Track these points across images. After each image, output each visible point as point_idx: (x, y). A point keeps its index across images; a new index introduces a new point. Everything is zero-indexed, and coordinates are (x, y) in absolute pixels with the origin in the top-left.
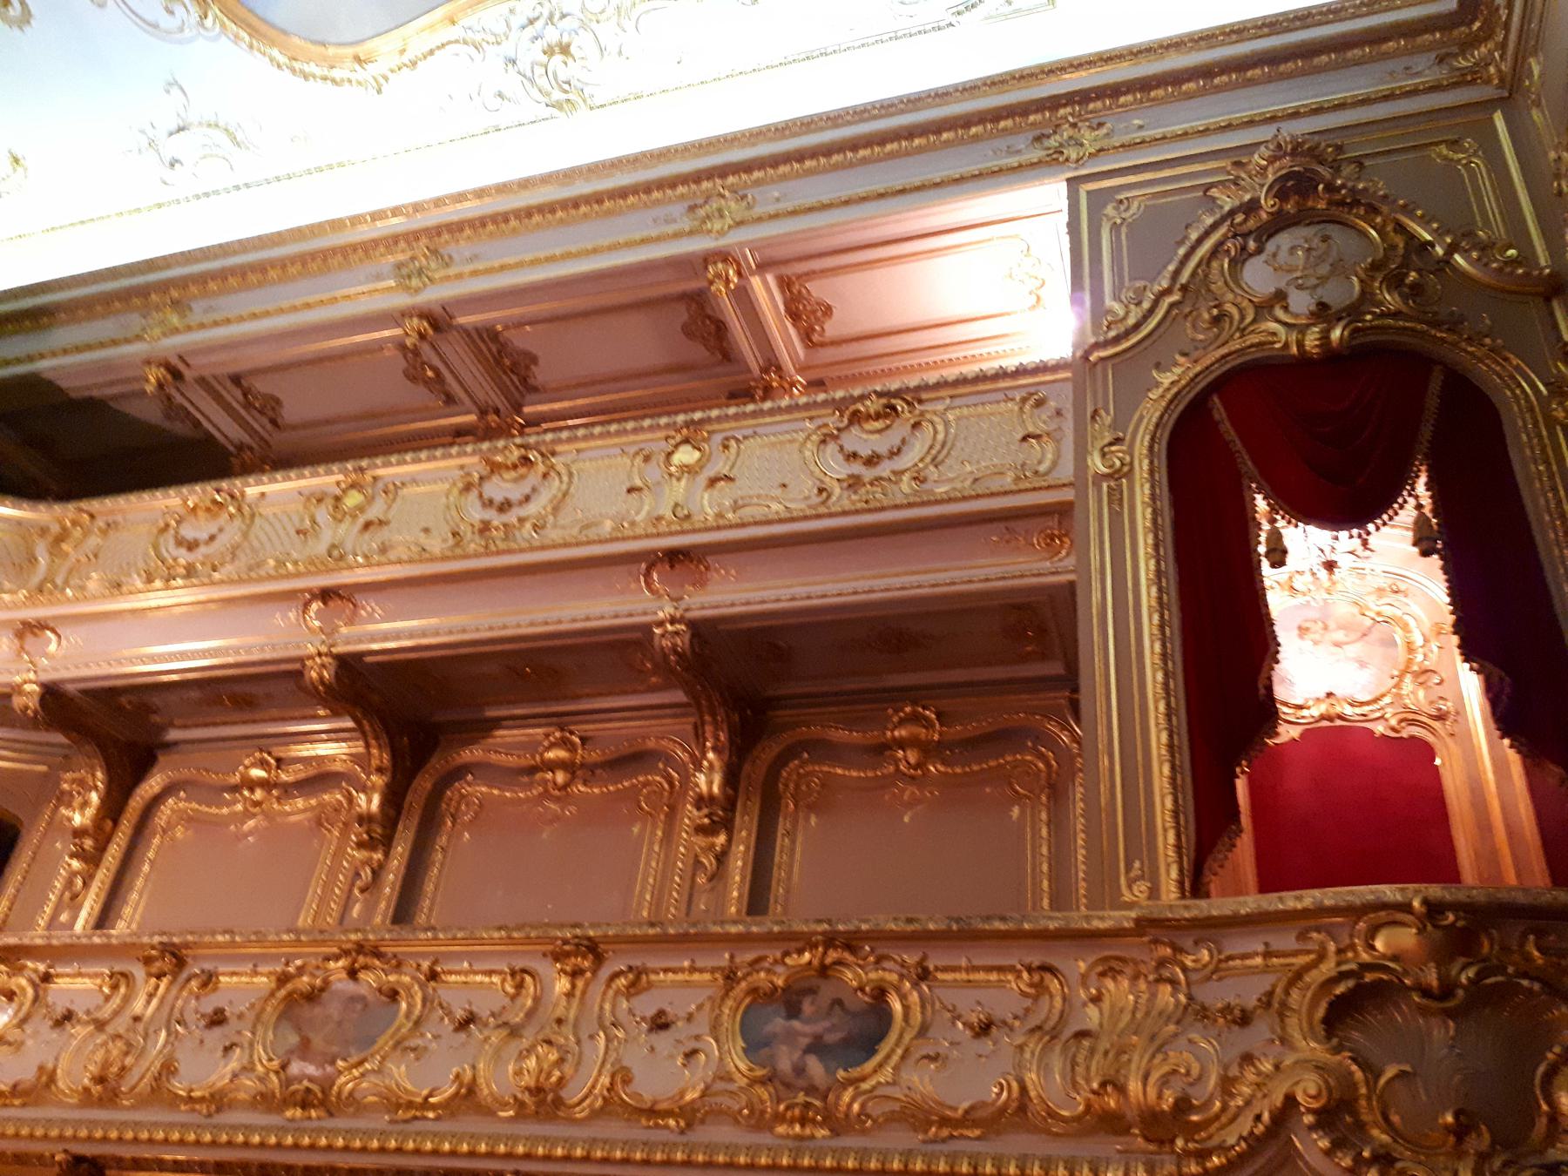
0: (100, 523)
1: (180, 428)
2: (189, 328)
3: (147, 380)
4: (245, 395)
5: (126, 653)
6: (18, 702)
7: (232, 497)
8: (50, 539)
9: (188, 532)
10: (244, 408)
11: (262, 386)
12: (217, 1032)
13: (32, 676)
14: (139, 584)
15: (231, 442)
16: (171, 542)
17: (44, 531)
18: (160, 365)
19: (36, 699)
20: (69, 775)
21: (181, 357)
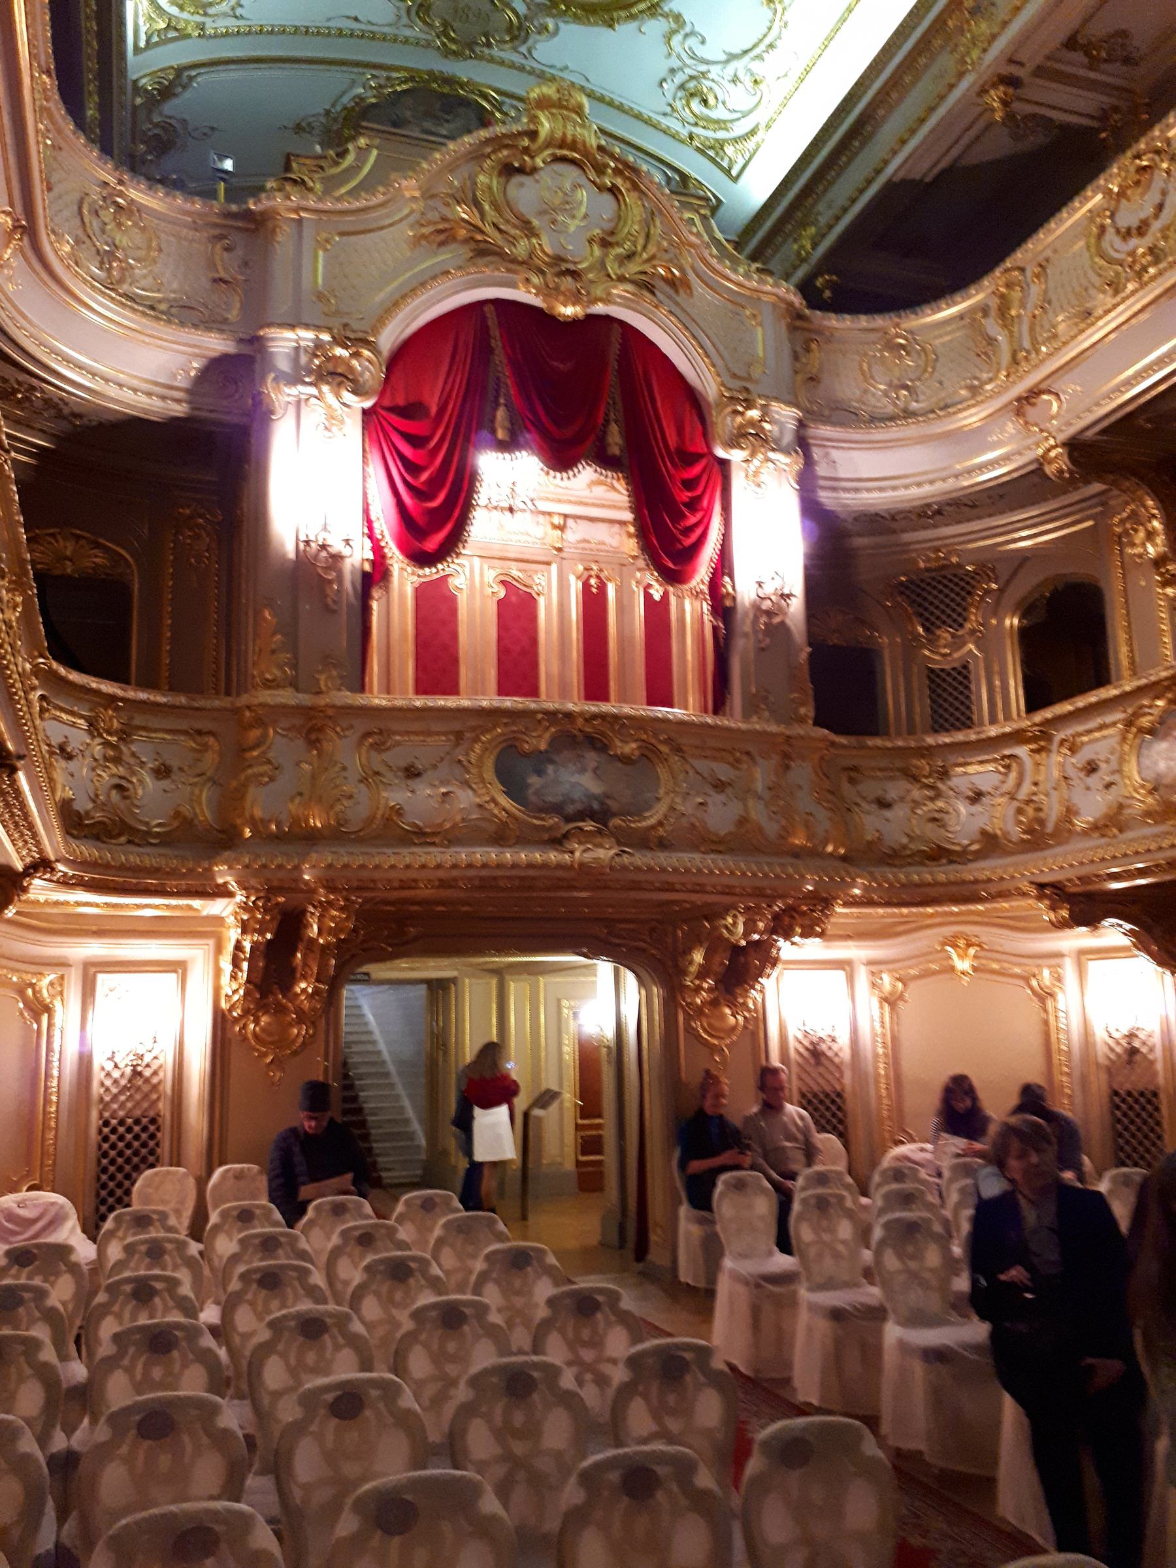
0: (1032, 269)
1: (1037, 139)
2: (1005, 24)
3: (993, 110)
4: (1087, 54)
5: (1106, 388)
7: (1158, 152)
9: (1128, 217)
10: (1091, 68)
11: (1099, 29)
13: (1052, 442)
14: (1110, 301)
15: (1092, 117)
16: (1118, 242)
17: (985, 310)
18: (994, 86)
20: (1116, 520)
21: (1011, 61)
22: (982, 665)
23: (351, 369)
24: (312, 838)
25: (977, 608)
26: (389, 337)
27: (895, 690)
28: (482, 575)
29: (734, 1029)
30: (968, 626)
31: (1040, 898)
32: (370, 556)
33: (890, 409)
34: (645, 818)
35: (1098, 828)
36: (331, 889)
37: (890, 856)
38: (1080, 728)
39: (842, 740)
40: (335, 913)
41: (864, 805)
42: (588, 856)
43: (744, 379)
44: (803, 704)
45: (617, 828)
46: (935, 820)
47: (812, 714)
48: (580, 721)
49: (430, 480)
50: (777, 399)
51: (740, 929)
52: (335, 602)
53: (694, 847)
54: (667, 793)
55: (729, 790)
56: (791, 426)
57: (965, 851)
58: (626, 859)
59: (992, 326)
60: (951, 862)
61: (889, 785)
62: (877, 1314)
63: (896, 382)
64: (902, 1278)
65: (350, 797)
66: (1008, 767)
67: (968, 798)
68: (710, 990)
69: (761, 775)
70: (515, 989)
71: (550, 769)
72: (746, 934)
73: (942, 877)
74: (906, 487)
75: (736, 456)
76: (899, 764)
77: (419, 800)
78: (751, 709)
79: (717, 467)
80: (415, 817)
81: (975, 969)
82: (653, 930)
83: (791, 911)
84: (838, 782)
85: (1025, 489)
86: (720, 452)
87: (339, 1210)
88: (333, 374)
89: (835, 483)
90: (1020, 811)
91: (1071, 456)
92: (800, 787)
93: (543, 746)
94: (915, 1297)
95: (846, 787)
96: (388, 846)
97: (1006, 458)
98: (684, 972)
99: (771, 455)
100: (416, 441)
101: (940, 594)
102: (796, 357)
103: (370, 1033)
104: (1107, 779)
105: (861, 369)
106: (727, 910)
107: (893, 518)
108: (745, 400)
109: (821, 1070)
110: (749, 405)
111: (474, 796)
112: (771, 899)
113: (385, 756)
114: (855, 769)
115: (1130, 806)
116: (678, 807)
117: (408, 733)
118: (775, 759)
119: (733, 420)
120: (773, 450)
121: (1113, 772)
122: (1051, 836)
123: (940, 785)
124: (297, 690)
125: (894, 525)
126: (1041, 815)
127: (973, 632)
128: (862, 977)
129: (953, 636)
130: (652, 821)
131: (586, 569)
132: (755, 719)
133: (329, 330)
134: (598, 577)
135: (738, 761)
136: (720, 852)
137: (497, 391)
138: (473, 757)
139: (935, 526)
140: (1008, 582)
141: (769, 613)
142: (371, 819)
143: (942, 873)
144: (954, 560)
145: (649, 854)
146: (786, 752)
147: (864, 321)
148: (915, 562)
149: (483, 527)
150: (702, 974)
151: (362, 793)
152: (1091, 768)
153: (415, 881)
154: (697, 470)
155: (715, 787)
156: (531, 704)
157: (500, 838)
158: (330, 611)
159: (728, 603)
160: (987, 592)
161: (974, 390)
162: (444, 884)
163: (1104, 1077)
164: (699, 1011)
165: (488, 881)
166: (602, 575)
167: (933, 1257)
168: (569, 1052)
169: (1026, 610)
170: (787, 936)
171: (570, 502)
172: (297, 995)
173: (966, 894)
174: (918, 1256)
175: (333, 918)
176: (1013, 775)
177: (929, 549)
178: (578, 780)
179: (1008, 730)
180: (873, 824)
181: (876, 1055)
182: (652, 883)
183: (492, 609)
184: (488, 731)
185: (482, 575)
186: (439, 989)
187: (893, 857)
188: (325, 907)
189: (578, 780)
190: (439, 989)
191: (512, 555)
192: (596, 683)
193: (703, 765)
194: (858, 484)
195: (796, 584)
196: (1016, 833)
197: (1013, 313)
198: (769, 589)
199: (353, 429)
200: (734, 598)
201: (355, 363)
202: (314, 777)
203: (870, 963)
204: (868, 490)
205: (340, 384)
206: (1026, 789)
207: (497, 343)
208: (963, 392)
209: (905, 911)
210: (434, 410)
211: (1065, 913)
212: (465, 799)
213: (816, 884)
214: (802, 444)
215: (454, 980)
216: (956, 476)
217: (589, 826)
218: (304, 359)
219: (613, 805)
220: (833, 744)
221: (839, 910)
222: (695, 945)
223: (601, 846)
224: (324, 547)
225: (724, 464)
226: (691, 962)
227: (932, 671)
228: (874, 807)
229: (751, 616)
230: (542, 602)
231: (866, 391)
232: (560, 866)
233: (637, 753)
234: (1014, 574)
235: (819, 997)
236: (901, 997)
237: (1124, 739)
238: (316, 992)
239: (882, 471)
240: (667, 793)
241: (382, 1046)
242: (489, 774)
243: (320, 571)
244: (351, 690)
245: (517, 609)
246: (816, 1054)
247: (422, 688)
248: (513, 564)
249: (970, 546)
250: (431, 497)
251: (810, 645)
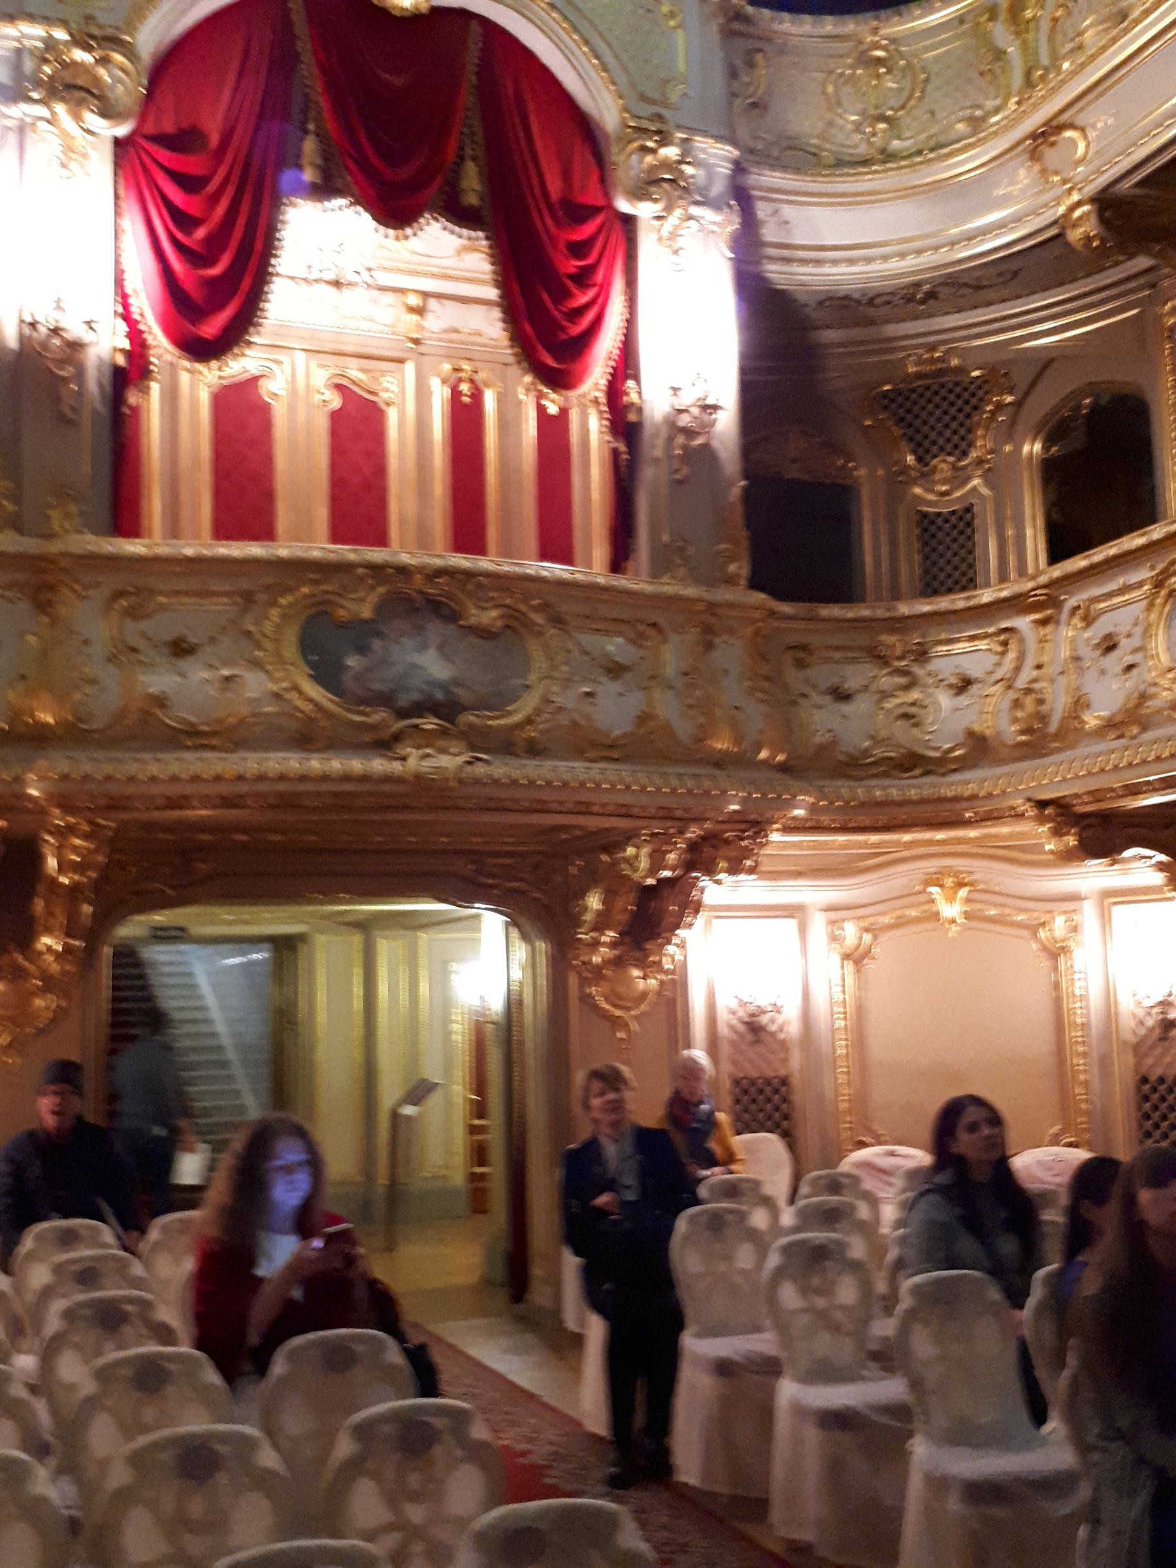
6: (1075, 236)
8: (1003, 16)
12: (1114, 655)
13: (1076, 197)
19: (1093, 219)
22: (990, 506)
23: (97, 80)
24: (41, 739)
25: (987, 429)
26: (153, 34)
27: (874, 543)
28: (308, 376)
29: (644, 995)
30: (974, 454)
31: (1041, 819)
32: (126, 344)
33: (863, 150)
34: (510, 713)
35: (1113, 726)
36: (67, 807)
37: (847, 765)
38: (1097, 591)
39: (786, 608)
40: (78, 842)
41: (816, 698)
42: (428, 764)
43: (653, 102)
44: (732, 559)
45: (471, 726)
46: (906, 716)
47: (745, 572)
48: (418, 579)
49: (209, 240)
50: (705, 133)
51: (644, 864)
52: (73, 408)
53: (578, 753)
54: (541, 679)
55: (628, 676)
56: (725, 169)
57: (943, 761)
58: (480, 769)
59: (1000, 32)
60: (928, 773)
61: (849, 670)
62: (771, 1368)
63: (872, 112)
64: (805, 1319)
65: (93, 681)
66: (1005, 644)
67: (951, 686)
68: (613, 945)
69: (672, 656)
70: (386, 948)
71: (377, 644)
72: (652, 871)
73: (913, 793)
74: (885, 258)
75: (644, 210)
76: (864, 640)
77: (190, 687)
78: (660, 566)
79: (618, 225)
80: (181, 714)
81: (967, 915)
82: (537, 866)
83: (711, 840)
84: (778, 666)
85: (1040, 264)
86: (623, 205)
87: (68, 1239)
88: (70, 87)
89: (789, 253)
90: (1017, 704)
91: (1102, 220)
92: (726, 672)
93: (366, 612)
94: (823, 1344)
95: (793, 676)
96: (144, 749)
97: (1017, 219)
98: (575, 922)
99: (694, 210)
100: (188, 183)
101: (938, 409)
102: (733, 74)
103: (203, 1008)
104: (1129, 659)
105: (824, 93)
106: (629, 837)
107: (871, 302)
108: (659, 132)
109: (761, 1049)
110: (665, 140)
111: (268, 680)
112: (684, 822)
113: (144, 625)
114: (804, 647)
115: (1153, 696)
116: (558, 699)
117: (177, 593)
118: (693, 633)
119: (641, 161)
120: (697, 203)
121: (1136, 651)
122: (1056, 736)
123: (917, 670)
124: (20, 531)
125: (871, 312)
126: (1044, 708)
127: (980, 462)
128: (818, 924)
129: (955, 468)
130: (517, 718)
131: (456, 370)
132: (665, 579)
133: (64, 23)
134: (472, 381)
135: (642, 636)
136: (616, 760)
137: (305, 112)
138: (268, 627)
139: (931, 316)
140: (1027, 394)
141: (689, 432)
142: (122, 713)
143: (915, 787)
144: (955, 362)
145: (515, 762)
146: (709, 625)
147: (829, 25)
148: (902, 362)
149: (283, 303)
150: (600, 925)
151: (109, 676)
152: (1109, 645)
153: (186, 797)
154: (589, 228)
155: (609, 671)
156: (376, 555)
157: (305, 738)
158: (66, 421)
159: (632, 417)
160: (1000, 407)
161: (977, 124)
162: (228, 802)
163: (1130, 1059)
164: (597, 974)
165: (288, 798)
166: (476, 377)
167: (847, 1292)
168: (460, 1032)
169: (1054, 433)
170: (710, 871)
171: (434, 276)
172: (40, 953)
173: (943, 813)
174: (826, 1291)
175: (75, 849)
176: (1012, 655)
177: (922, 346)
178: (428, 662)
179: (1004, 594)
180: (824, 721)
181: (834, 1031)
182: (517, 801)
183: (322, 424)
184: (290, 590)
185: (308, 376)
186: (285, 948)
187: (853, 766)
188: (63, 833)
189: (428, 662)
190: (285, 948)
191: (349, 349)
192: (468, 530)
193: (590, 641)
194: (819, 253)
195: (725, 392)
196: (1011, 732)
197: (1029, 14)
198: (687, 399)
199: (100, 168)
200: (640, 410)
201: (102, 72)
202: (44, 653)
203: (829, 908)
204: (835, 262)
205: (80, 103)
206: (1027, 674)
207: (304, 47)
208: (961, 127)
209: (874, 838)
210: (214, 140)
211: (1071, 841)
212: (255, 684)
213: (744, 801)
214: (741, 197)
215: (301, 938)
216: (953, 244)
217: (430, 723)
218: (29, 65)
219: (464, 695)
220: (772, 613)
221: (775, 837)
222: (606, 890)
223: (444, 751)
224: (56, 331)
225: (629, 221)
226: (586, 909)
227: (925, 515)
228: (827, 699)
229: (664, 434)
230: (392, 416)
231: (831, 124)
232: (388, 779)
233: (500, 623)
234: (1033, 385)
235: (760, 954)
236: (868, 953)
237: (1150, 606)
238: (68, 949)
239: (856, 236)
240: (541, 679)
241: (221, 1027)
242: (291, 650)
243: (51, 366)
244: (96, 533)
245: (356, 426)
246: (755, 1029)
247: (223, 530)
248: (353, 362)
249: (963, 344)
250: (211, 262)
251: (746, 478)
